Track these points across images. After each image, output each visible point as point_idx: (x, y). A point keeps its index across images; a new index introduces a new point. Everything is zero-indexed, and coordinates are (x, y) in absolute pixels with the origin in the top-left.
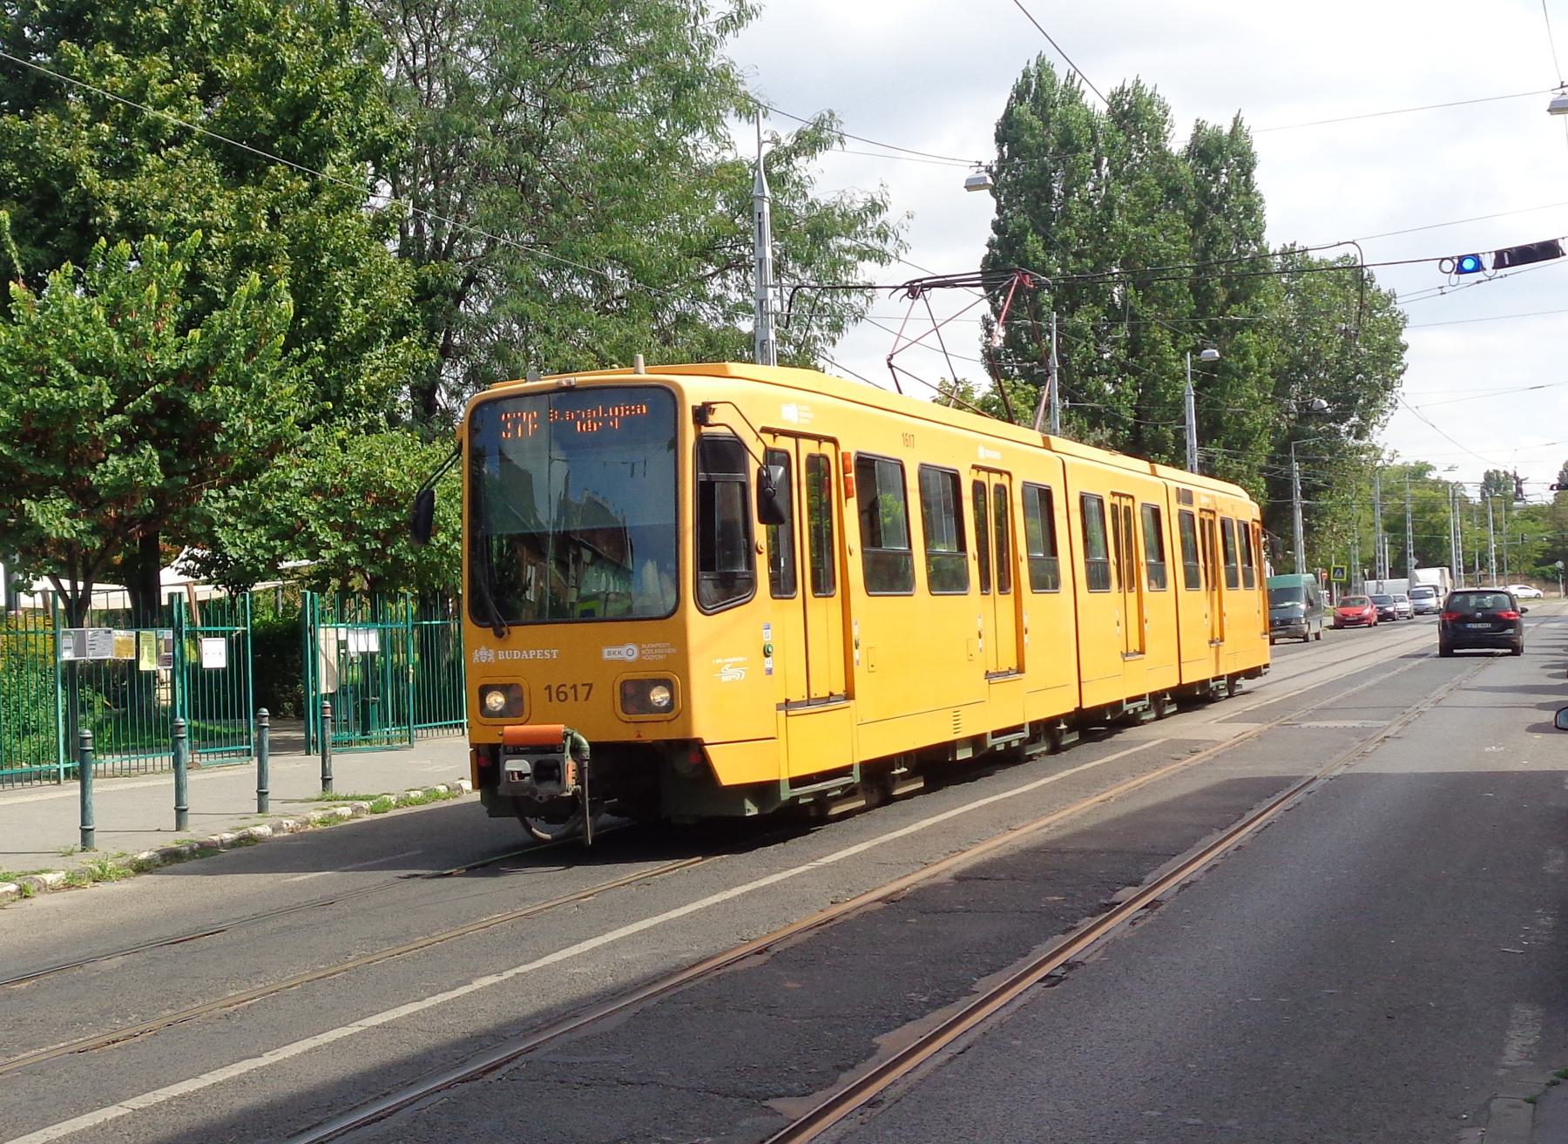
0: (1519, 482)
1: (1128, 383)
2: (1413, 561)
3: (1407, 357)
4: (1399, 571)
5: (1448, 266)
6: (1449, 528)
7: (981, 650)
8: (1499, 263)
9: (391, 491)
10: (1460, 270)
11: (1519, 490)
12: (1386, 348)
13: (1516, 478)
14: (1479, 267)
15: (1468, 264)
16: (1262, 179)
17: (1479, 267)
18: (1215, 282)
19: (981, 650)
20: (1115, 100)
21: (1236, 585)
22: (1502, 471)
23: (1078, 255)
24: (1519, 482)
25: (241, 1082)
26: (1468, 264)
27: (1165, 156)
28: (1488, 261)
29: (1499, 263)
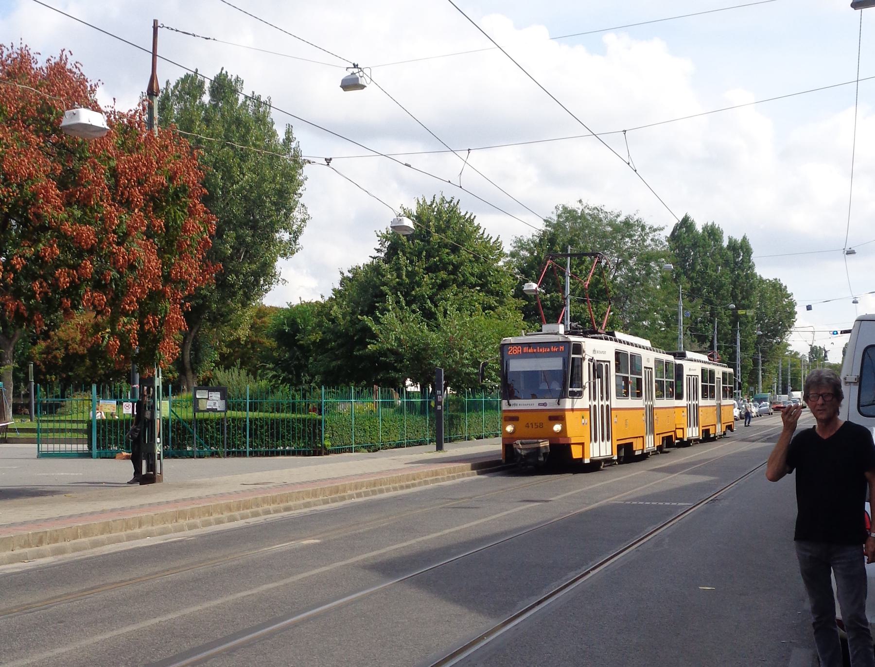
0: (826, 352)
1: (710, 326)
2: (790, 388)
3: (797, 316)
4: (785, 392)
5: (831, 333)
6: (801, 374)
7: (583, 418)
8: (841, 333)
9: (428, 344)
10: (834, 334)
11: (826, 356)
12: (790, 313)
13: (825, 350)
14: (837, 334)
15: (835, 333)
16: (754, 258)
17: (837, 334)
18: (738, 292)
19: (583, 418)
20: (705, 228)
21: (168, 395)
22: (818, 346)
23: (696, 283)
24: (826, 352)
25: (374, 557)
26: (835, 333)
27: (722, 248)
28: (839, 332)
29: (841, 333)
